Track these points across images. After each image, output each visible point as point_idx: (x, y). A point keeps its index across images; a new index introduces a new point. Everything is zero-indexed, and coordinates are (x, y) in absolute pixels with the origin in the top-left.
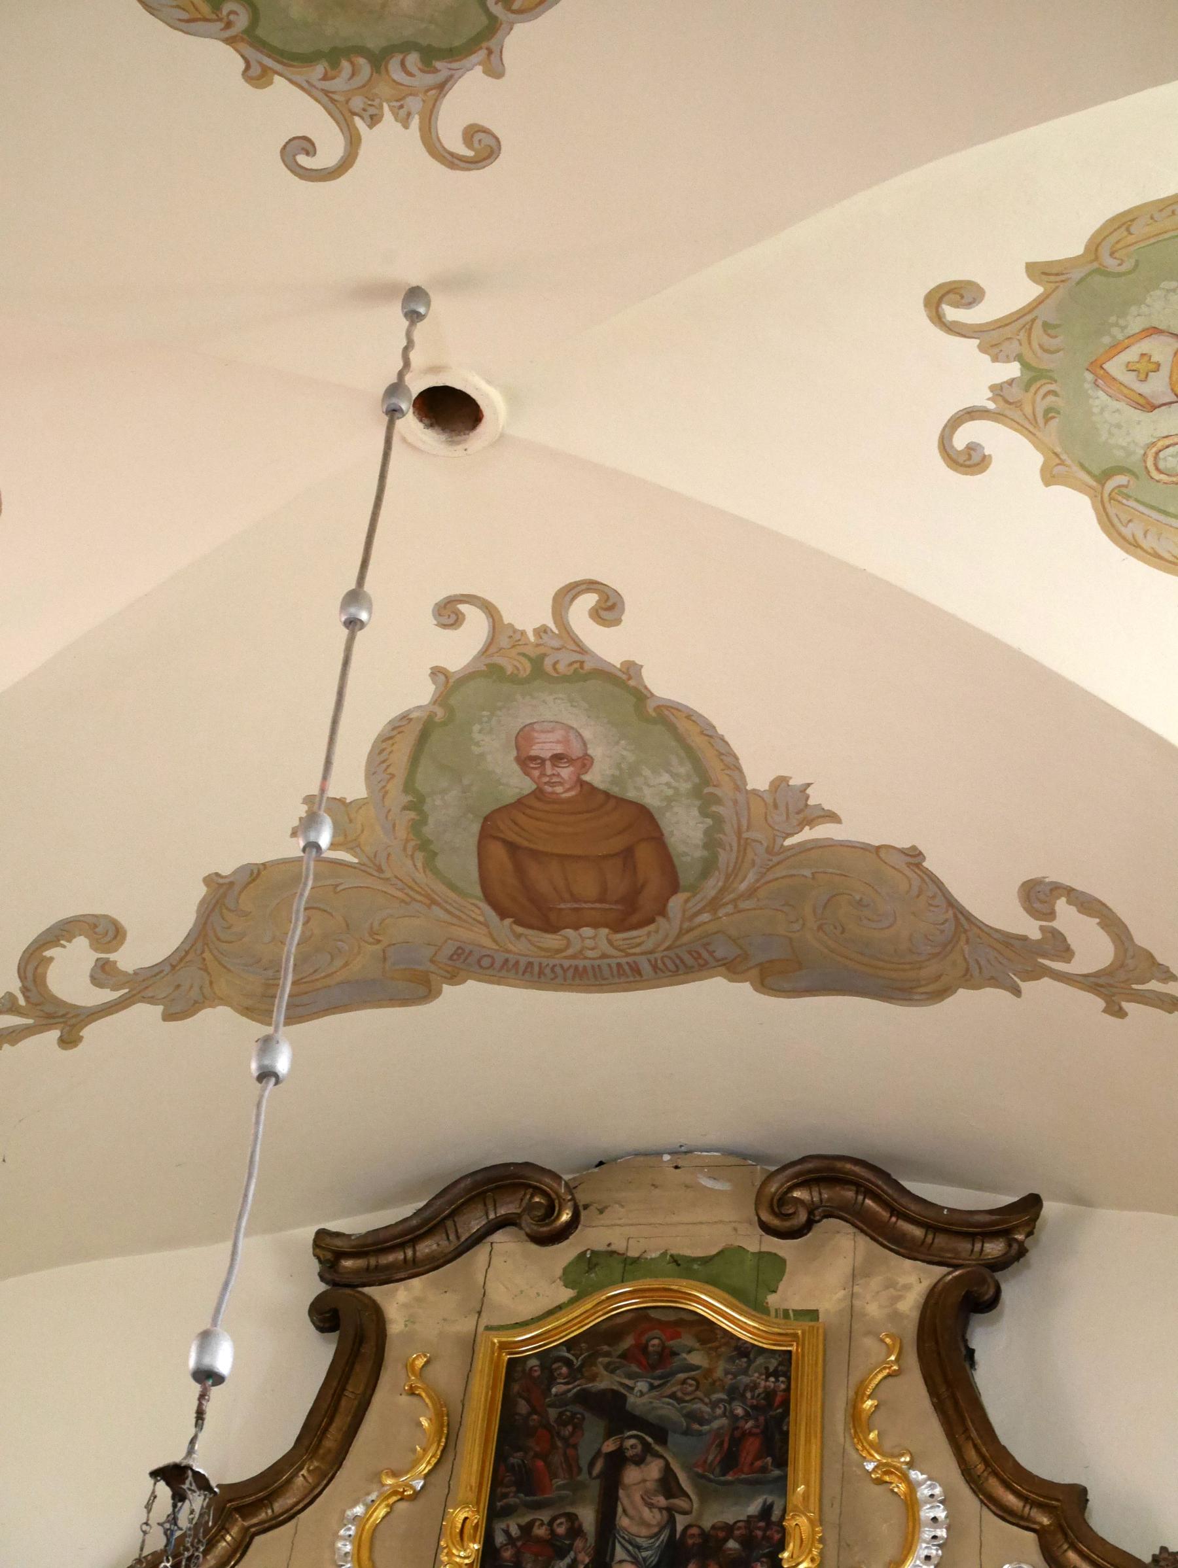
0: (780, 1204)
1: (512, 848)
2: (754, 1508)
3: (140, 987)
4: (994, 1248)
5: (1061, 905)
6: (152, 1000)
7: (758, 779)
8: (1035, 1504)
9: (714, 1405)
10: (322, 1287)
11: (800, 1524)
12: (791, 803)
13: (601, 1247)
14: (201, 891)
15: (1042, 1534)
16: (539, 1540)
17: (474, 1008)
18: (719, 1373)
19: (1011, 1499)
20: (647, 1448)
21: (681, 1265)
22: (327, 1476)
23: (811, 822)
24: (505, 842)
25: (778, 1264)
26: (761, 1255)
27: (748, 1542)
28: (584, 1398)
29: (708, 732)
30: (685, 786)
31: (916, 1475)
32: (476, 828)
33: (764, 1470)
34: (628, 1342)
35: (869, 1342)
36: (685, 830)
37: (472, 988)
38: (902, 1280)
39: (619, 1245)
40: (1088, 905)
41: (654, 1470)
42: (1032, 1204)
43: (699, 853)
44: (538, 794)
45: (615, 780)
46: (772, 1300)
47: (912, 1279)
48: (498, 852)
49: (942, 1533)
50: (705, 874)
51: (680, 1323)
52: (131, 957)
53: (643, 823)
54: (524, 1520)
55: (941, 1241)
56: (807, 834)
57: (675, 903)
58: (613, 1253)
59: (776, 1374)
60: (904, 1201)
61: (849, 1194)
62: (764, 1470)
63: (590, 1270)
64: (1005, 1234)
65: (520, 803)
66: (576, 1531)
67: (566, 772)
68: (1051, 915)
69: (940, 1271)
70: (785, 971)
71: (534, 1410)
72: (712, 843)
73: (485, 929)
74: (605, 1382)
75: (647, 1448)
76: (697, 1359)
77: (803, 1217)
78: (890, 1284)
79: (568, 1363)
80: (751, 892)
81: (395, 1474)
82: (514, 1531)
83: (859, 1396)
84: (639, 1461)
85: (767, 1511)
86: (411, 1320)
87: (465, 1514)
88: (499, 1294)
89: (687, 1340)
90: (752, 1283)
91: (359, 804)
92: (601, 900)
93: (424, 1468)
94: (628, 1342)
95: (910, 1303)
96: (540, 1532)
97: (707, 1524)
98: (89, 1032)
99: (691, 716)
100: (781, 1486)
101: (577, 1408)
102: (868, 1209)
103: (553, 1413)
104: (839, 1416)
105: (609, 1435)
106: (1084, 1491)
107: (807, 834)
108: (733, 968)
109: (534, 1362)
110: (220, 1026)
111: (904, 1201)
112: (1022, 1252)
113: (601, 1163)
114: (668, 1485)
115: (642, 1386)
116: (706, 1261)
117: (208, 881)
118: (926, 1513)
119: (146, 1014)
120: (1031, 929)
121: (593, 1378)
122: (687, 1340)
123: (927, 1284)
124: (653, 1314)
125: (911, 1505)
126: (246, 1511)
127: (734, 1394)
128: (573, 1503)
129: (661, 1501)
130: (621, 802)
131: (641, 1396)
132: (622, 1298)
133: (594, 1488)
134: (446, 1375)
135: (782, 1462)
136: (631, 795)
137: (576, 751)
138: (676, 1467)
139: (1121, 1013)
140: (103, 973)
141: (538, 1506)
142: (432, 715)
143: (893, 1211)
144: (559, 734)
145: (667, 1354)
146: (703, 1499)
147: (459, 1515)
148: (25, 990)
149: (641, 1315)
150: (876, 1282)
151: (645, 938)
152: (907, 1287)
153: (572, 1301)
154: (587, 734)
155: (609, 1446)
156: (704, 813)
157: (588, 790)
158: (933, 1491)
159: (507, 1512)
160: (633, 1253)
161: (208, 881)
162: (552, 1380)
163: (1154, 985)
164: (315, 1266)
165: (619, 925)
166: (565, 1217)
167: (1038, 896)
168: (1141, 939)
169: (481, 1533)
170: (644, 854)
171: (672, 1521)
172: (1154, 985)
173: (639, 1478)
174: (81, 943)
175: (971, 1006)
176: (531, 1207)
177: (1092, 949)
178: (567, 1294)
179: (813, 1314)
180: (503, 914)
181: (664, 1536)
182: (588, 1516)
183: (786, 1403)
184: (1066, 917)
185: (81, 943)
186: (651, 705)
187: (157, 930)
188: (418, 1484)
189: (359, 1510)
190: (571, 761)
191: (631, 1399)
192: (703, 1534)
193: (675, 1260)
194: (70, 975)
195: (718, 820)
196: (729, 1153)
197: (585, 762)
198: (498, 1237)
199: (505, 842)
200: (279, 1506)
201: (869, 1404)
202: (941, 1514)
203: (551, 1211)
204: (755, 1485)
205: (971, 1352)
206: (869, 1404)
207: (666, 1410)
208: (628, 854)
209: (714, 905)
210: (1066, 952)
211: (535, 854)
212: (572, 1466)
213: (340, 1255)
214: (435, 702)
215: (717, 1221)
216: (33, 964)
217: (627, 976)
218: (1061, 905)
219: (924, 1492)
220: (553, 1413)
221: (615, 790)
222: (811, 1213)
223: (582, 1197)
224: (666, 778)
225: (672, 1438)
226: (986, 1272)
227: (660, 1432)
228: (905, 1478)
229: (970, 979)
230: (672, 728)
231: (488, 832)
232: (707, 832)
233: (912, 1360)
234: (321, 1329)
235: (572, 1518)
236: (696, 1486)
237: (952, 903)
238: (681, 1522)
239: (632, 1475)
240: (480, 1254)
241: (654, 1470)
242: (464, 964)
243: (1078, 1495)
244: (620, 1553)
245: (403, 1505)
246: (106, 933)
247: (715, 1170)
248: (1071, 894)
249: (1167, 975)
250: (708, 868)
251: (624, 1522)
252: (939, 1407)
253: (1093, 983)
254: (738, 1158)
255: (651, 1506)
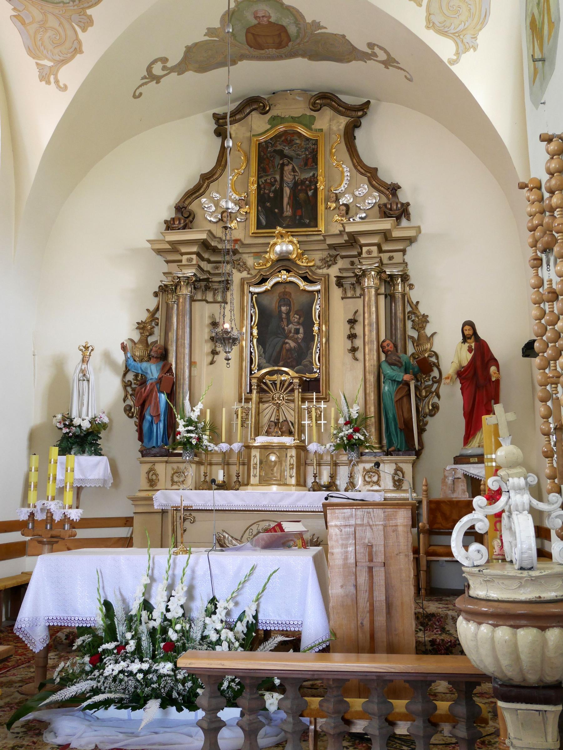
0: (314, 104)
1: (253, 34)
2: (311, 174)
3: (172, 70)
4: (360, 113)
5: (376, 47)
6: (175, 72)
7: (309, 20)
8: (367, 172)
9: (302, 152)
10: (216, 126)
11: (320, 178)
12: (316, 25)
13: (275, 115)
14: (185, 49)
15: (368, 177)
16: (268, 183)
17: (245, 66)
18: (303, 145)
19: (362, 171)
20: (289, 162)
21: (293, 119)
22: (223, 170)
23: (321, 29)
24: (252, 33)
25: (314, 118)
26: (310, 116)
27: (310, 182)
28: (275, 151)
29: (297, 11)
30: (292, 21)
31: (344, 166)
32: (245, 31)
33: (313, 166)
34: (283, 138)
35: (334, 136)
36: (292, 30)
37: (245, 62)
38: (341, 121)
39: (279, 114)
40: (381, 48)
41: (290, 167)
42: (368, 102)
43: (295, 34)
44: (259, 23)
45: (276, 20)
46: (313, 126)
47: (342, 121)
48: (250, 36)
49: (349, 178)
50: (297, 38)
51: (294, 133)
52: (169, 65)
53: (283, 29)
54: (265, 179)
55: (348, 112)
56: (320, 31)
57: (290, 44)
58: (278, 116)
59: (314, 144)
60: (341, 103)
61: (329, 101)
62: (313, 166)
63: (275, 121)
64: (363, 110)
65: (255, 26)
66: (276, 181)
67: (265, 19)
68: (374, 49)
69: (349, 118)
70: (314, 56)
71: (265, 154)
72: (298, 32)
73: (246, 49)
74: (279, 147)
75: (289, 162)
76: (298, 141)
77: (319, 107)
78: (338, 122)
79: (271, 143)
80: (307, 42)
81: (237, 169)
82: (263, 181)
83: (332, 149)
84: (287, 165)
85: (314, 175)
86: (236, 134)
87: (253, 179)
88: (254, 127)
89: (296, 137)
90: (308, 122)
91: (218, 28)
92: (273, 43)
93: (243, 168)
94: (283, 138)
95: (342, 127)
96: (269, 181)
97: (302, 178)
98: (162, 80)
99: (294, 8)
100: (316, 169)
101: (274, 154)
102: (333, 105)
103: (269, 155)
104: (328, 153)
105: (281, 159)
106: (377, 168)
107: (320, 31)
108: (303, 56)
109: (264, 143)
110: (190, 74)
111: (341, 103)
112: (366, 113)
113: (274, 93)
114: (294, 170)
115: (287, 148)
116: (298, 117)
117: (186, 47)
118: (346, 174)
119: (174, 75)
120: (369, 51)
121: (276, 147)
122: (296, 137)
123: (346, 122)
124: (288, 131)
125: (342, 172)
126: (208, 179)
127: (306, 149)
128: (275, 175)
129: (293, 174)
130: (277, 24)
131: (287, 150)
132: (281, 128)
133: (279, 170)
134: (245, 146)
135: (317, 164)
136: (280, 23)
137: (267, 15)
138: (295, 166)
139: (388, 68)
140: (164, 68)
141: (267, 176)
142: (234, 10)
143: (338, 105)
144: (264, 12)
145: (291, 141)
146: (301, 173)
147: (252, 179)
148: (148, 74)
149: (285, 131)
150: (335, 121)
151: (283, 50)
152: (342, 123)
153: (271, 128)
154: (270, 12)
155: (281, 162)
156: (297, 26)
157: (270, 23)
158: (347, 169)
159: (261, 177)
160: (283, 116)
161: (186, 47)
162: (268, 147)
163: (395, 64)
164: (214, 121)
165: (277, 48)
166: (267, 109)
167: (371, 45)
168: (393, 55)
169: (256, 183)
170: (283, 35)
171: (295, 178)
172: (395, 64)
173: (288, 169)
174: (159, 63)
175: (355, 64)
176: (260, 107)
177: (382, 56)
178: (269, 127)
179: (321, 130)
180: (251, 47)
181: (294, 181)
182: (278, 177)
183: (317, 151)
184: (377, 50)
185: (159, 63)
186: (284, 6)
187: (175, 59)
188: (242, 171)
189: (231, 177)
190: (266, 17)
191: (285, 151)
192: (301, 181)
193: (292, 118)
194: (157, 70)
195: (300, 28)
196: (302, 90)
197: (270, 17)
198: (253, 113)
199: (252, 33)
200: (214, 177)
201: (334, 150)
202: (349, 174)
203: (264, 107)
204: (311, 169)
205: (355, 137)
206: (334, 150)
207: (292, 153)
208: (279, 35)
209: (299, 44)
210: (377, 56)
211: (258, 35)
212: (274, 166)
213: (219, 119)
214: (235, 6)
215: (299, 108)
216: (149, 69)
217: (280, 57)
218: (376, 47)
219: (345, 170)
220: (269, 155)
221: (276, 22)
222: (321, 105)
223: (271, 103)
224: (288, 20)
225: (294, 160)
226: (358, 119)
227: (291, 158)
228: (341, 167)
229: (356, 59)
230: (289, 10)
231: (248, 31)
232: (298, 30)
233: (343, 140)
234: (217, 136)
235: (275, 178)
236: (299, 170)
237: (352, 45)
238: (297, 178)
239: (286, 168)
240: (249, 117)
241: (290, 167)
242: (242, 57)
243: (376, 169)
244: (285, 185)
245: (240, 176)
246: (164, 60)
247: (299, 95)
248: (377, 46)
249: (398, 63)
250: (297, 37)
251: (285, 178)
252: (348, 151)
253: (383, 62)
254: (304, 91)
255: (290, 175)
